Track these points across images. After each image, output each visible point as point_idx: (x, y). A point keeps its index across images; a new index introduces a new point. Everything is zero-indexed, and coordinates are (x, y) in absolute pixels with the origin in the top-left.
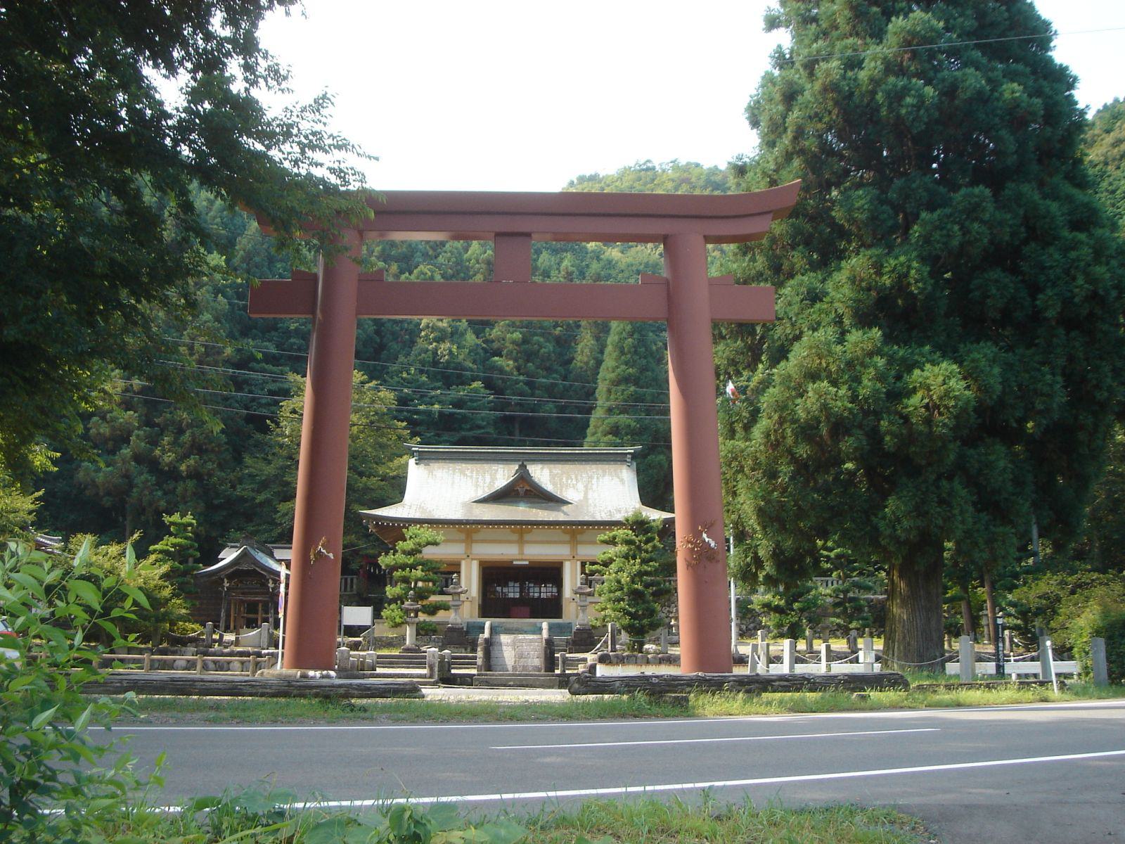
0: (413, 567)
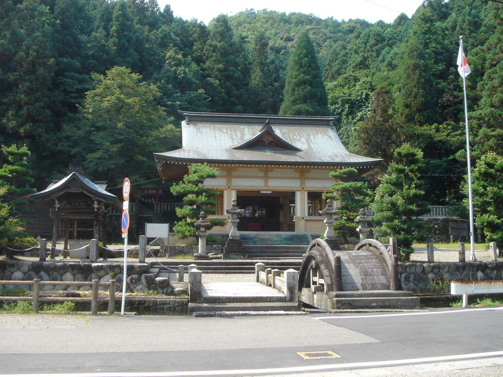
0: (198, 194)
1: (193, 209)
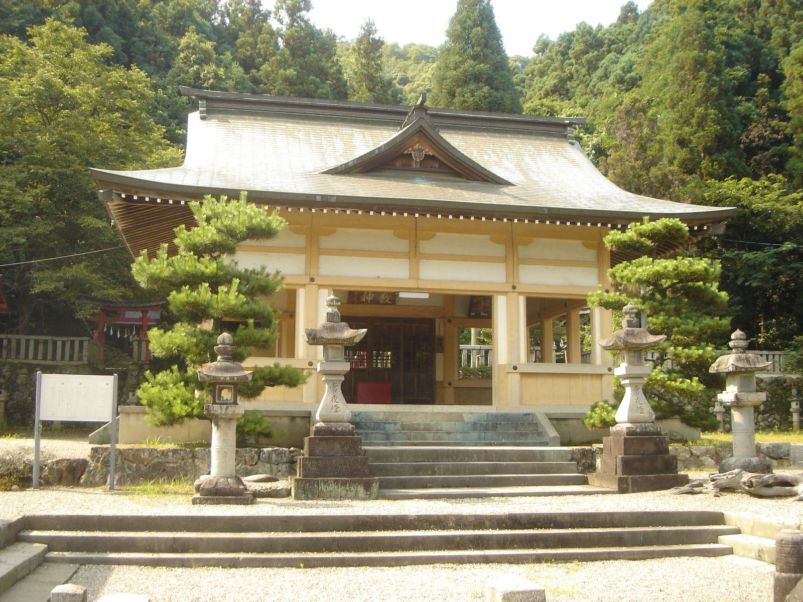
0: (215, 282)
1: (203, 332)
